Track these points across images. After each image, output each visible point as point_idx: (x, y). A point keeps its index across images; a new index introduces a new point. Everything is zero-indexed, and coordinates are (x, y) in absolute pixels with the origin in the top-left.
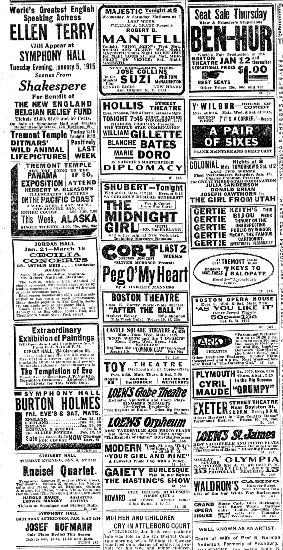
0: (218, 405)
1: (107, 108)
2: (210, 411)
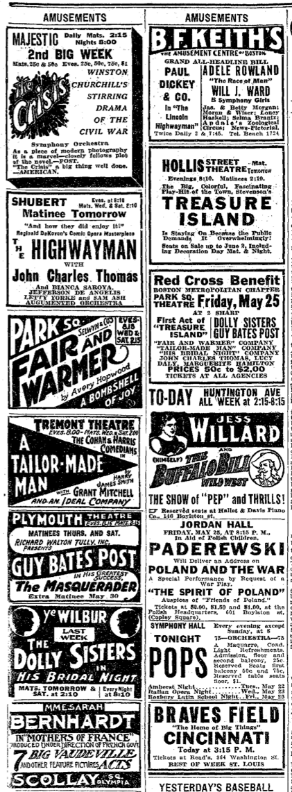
1: (242, 572)
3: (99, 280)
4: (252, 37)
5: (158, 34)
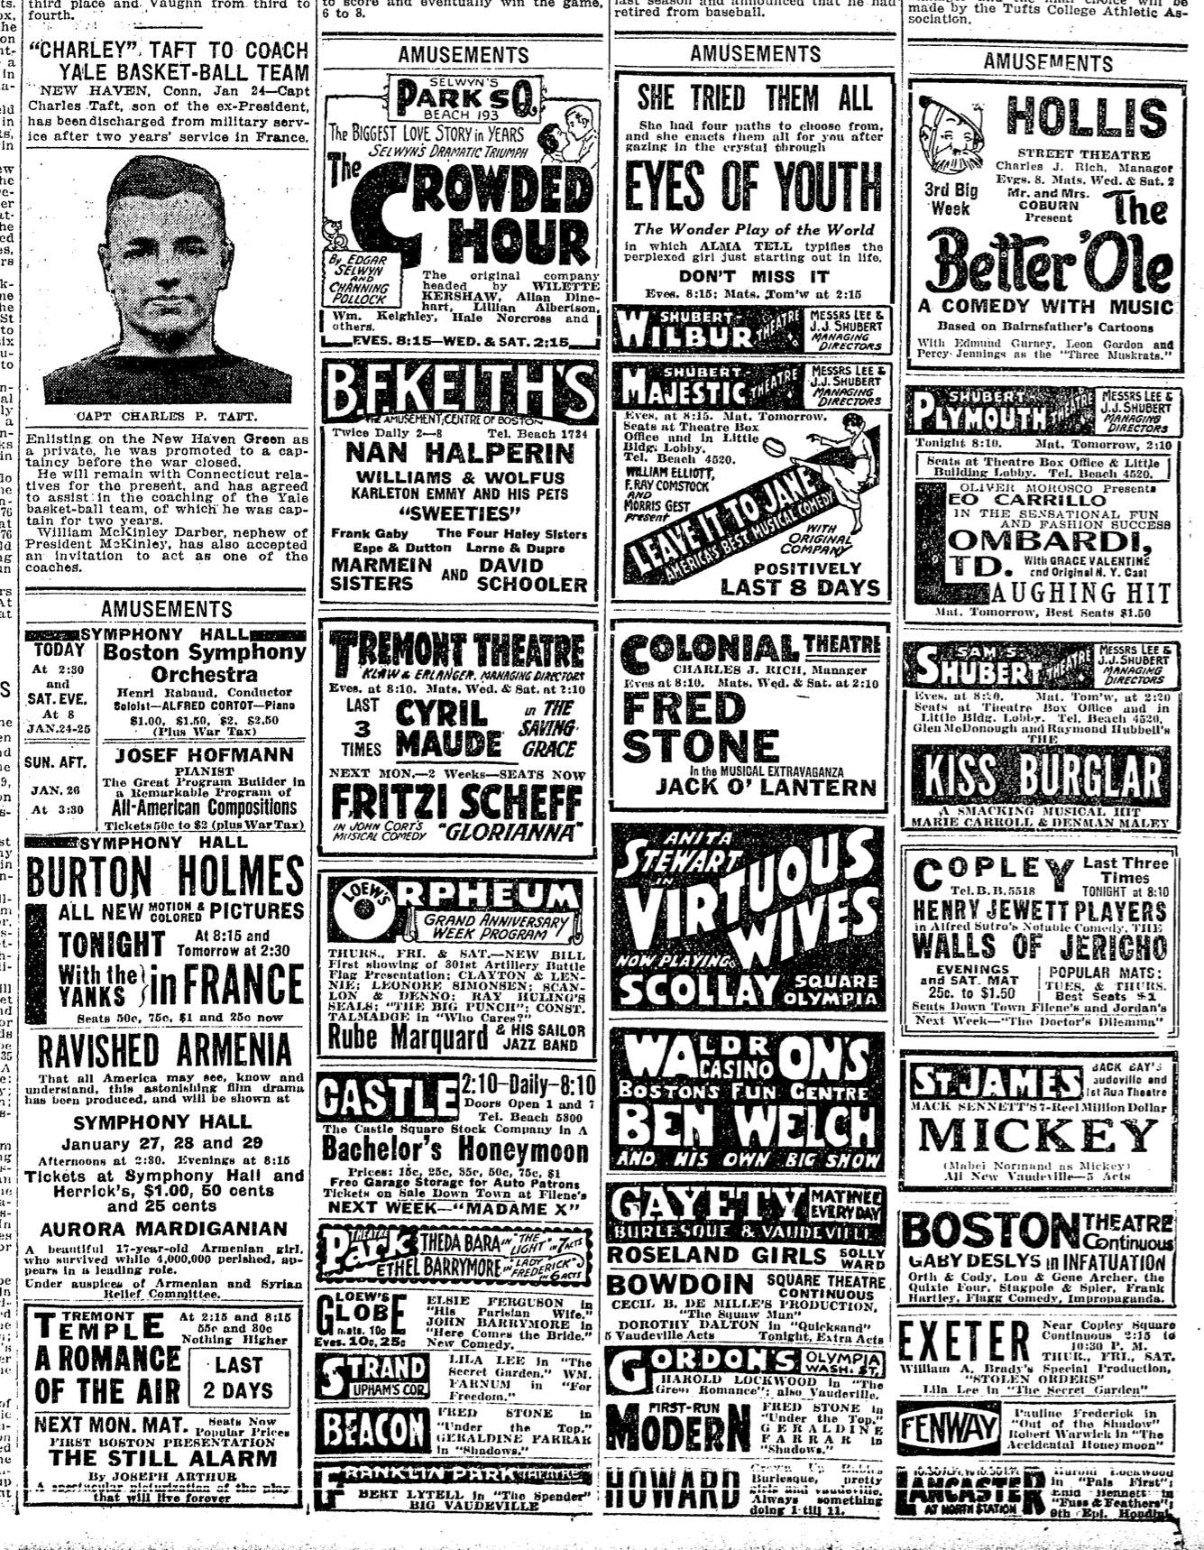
2: (961, 1348)
3: (84, 1400)
4: (524, 387)
5: (340, 376)
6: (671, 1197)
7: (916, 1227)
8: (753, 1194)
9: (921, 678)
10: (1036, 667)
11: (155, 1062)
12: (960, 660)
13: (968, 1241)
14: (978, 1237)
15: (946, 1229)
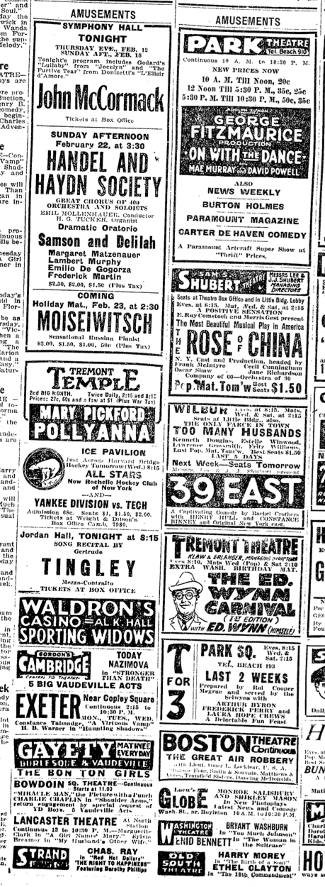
0: (62, 701)
6: (47, 747)
7: (170, 742)
8: (87, 744)
9: (181, 287)
10: (237, 282)
11: (145, 171)
12: (199, 278)
13: (196, 749)
14: (200, 746)
15: (185, 743)
